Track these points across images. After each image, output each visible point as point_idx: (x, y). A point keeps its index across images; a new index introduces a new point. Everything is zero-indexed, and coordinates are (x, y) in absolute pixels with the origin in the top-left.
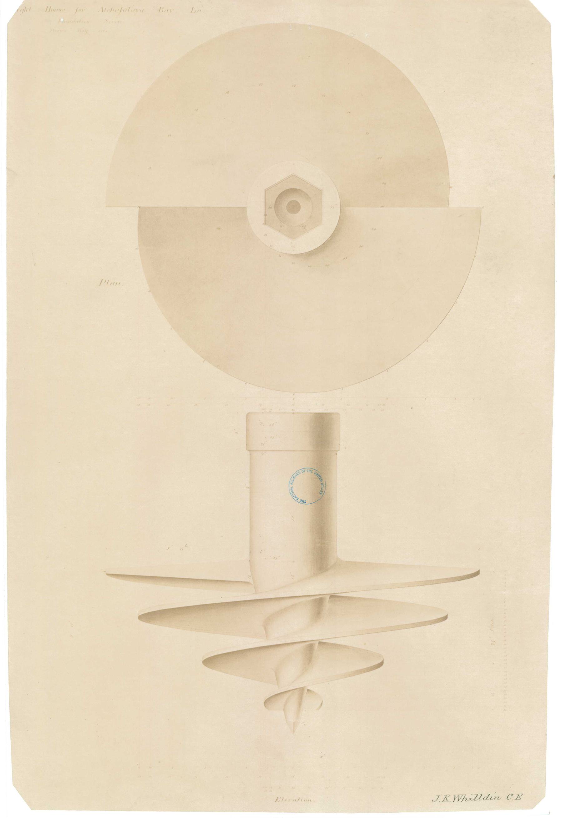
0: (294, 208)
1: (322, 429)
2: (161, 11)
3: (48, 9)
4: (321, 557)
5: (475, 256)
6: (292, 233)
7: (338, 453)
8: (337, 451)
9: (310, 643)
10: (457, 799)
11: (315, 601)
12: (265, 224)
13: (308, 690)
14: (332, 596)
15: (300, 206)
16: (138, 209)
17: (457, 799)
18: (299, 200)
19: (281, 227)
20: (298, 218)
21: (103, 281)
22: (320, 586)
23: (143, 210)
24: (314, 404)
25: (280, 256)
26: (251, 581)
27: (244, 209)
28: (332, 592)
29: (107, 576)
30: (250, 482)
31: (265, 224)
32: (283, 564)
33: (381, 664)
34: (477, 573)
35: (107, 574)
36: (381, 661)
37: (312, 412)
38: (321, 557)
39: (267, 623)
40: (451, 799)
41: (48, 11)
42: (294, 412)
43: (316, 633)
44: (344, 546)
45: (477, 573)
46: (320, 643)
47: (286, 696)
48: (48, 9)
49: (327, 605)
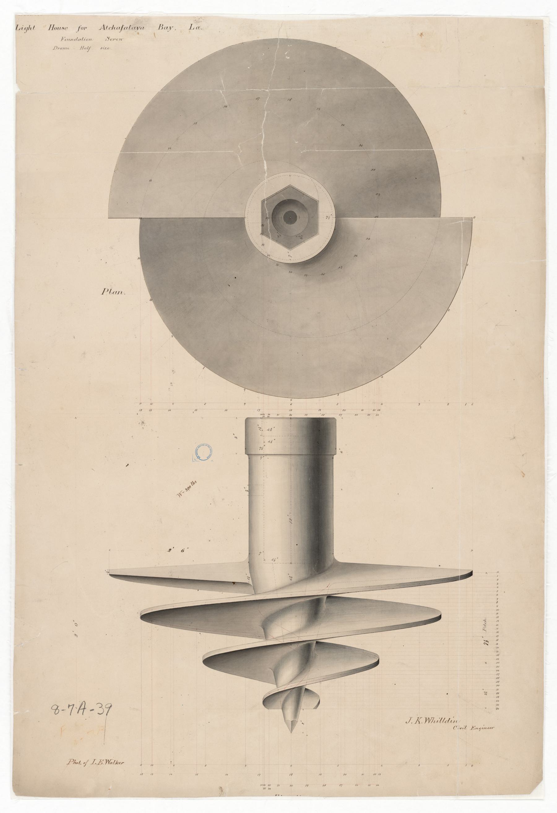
0: (291, 218)
1: (318, 437)
2: (161, 28)
3: (52, 26)
4: (317, 553)
5: (467, 265)
6: (290, 243)
7: (335, 457)
8: (333, 455)
9: (307, 643)
10: (428, 721)
11: (312, 601)
12: (262, 233)
13: (306, 689)
14: (329, 597)
15: (296, 216)
16: (139, 220)
17: (428, 721)
18: (296, 210)
19: (278, 236)
20: (296, 228)
21: (106, 290)
22: (318, 588)
23: (147, 226)
24: (314, 408)
25: (277, 265)
26: (251, 583)
27: (241, 221)
28: (329, 593)
29: (110, 577)
30: (249, 485)
31: (262, 233)
32: (279, 571)
33: (377, 663)
34: (470, 574)
35: (110, 575)
36: (376, 660)
37: (308, 416)
38: (317, 553)
39: (266, 624)
40: (422, 720)
41: (51, 28)
42: (292, 417)
43: (312, 635)
44: (341, 549)
45: (470, 574)
46: (317, 642)
47: (285, 695)
48: (52, 26)
49: (324, 605)
